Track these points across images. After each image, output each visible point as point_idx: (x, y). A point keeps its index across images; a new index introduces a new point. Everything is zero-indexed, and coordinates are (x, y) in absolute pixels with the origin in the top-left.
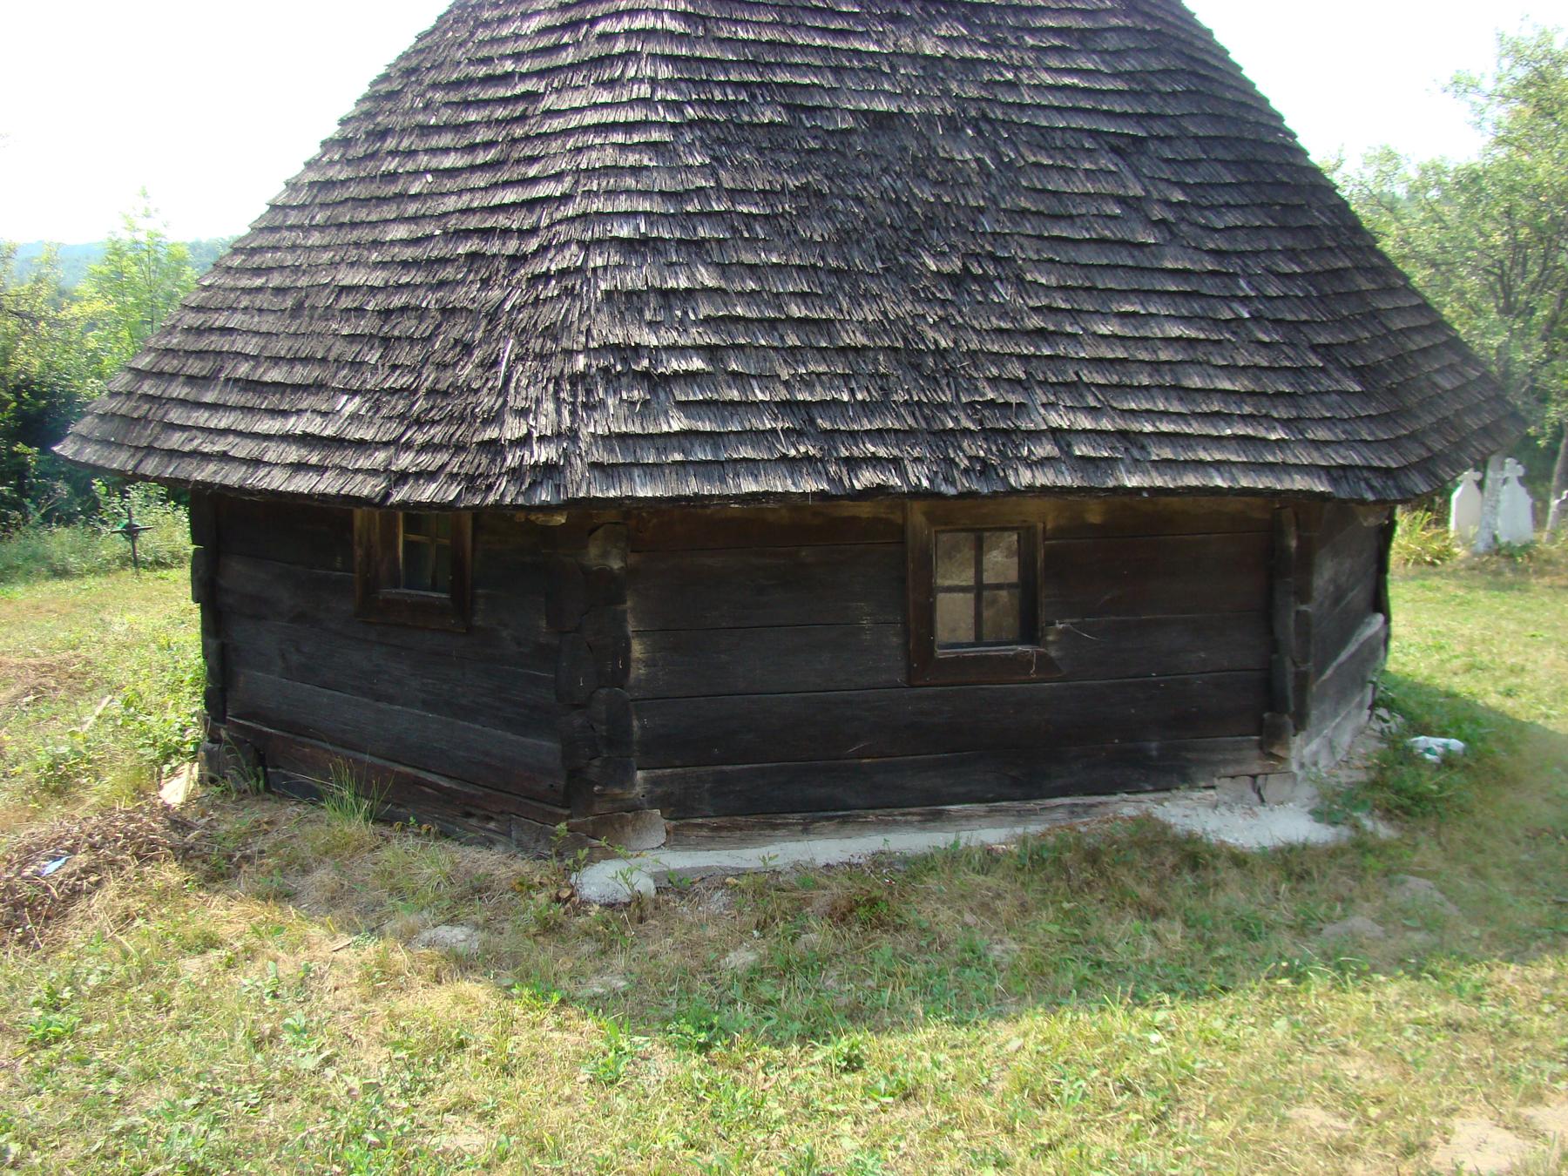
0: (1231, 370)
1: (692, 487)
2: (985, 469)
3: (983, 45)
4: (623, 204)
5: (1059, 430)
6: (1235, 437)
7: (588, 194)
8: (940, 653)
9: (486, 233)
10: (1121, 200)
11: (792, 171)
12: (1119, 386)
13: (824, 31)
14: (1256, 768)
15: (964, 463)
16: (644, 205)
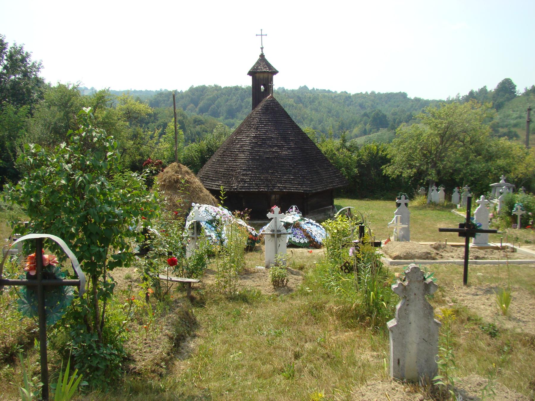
2: (272, 189)
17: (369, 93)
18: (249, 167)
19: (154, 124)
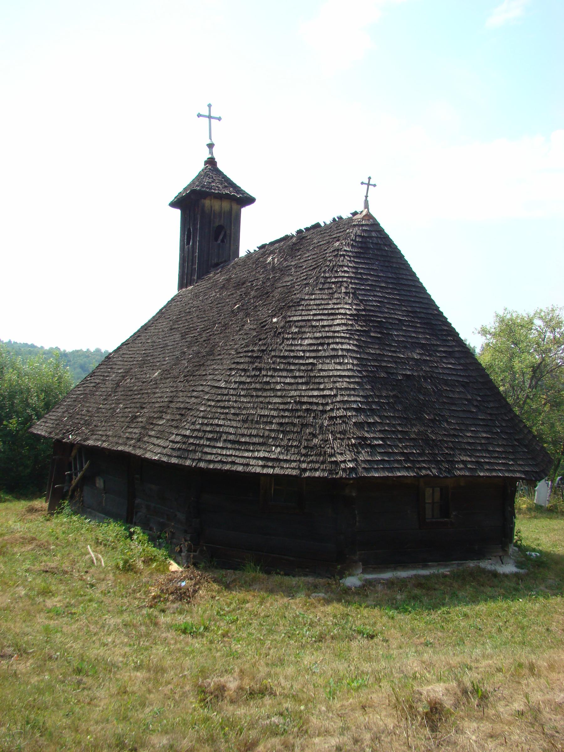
0: (498, 446)
1: (387, 474)
3: (428, 356)
4: (353, 399)
5: (463, 461)
6: (502, 463)
7: (342, 395)
8: (427, 521)
9: (311, 403)
10: (466, 400)
11: (391, 391)
12: (474, 449)
13: (390, 351)
14: (501, 554)
15: (444, 469)
16: (358, 399)
17: (92, 350)
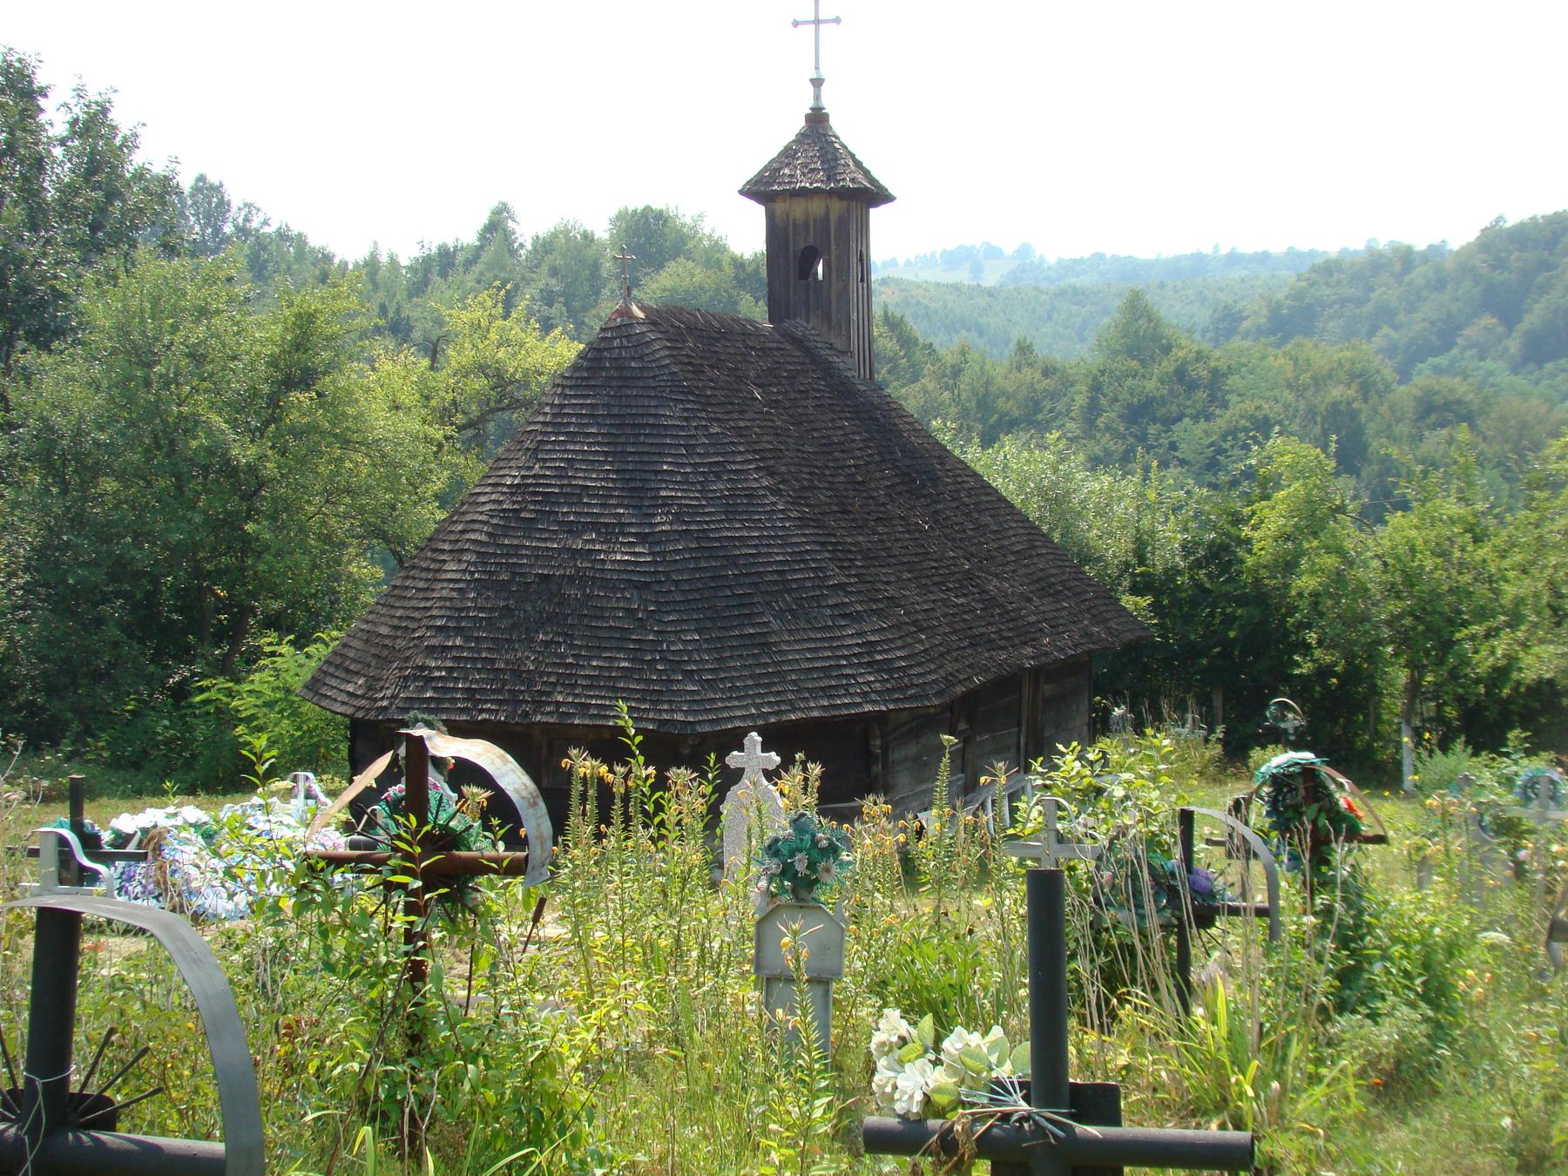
2: (526, 714)
18: (460, 619)
19: (1203, 424)
